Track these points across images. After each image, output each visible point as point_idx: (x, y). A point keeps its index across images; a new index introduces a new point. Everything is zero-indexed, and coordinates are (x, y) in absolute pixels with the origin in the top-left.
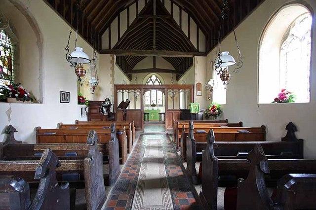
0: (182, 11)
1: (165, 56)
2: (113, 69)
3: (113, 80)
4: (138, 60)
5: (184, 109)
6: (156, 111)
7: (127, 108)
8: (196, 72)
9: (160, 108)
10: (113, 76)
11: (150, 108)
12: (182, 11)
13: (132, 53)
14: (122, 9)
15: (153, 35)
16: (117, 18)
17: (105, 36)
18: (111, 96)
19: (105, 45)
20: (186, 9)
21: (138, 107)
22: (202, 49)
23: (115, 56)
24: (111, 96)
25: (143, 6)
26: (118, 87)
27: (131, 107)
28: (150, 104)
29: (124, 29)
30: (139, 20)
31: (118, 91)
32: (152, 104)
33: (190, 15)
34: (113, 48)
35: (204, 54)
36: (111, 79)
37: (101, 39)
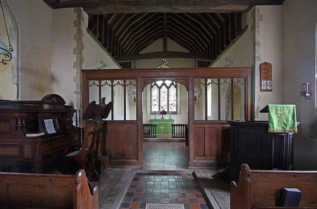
2: (79, 38)
3: (81, 60)
6: (166, 120)
7: (109, 118)
8: (259, 38)
9: (173, 117)
10: (79, 51)
11: (159, 117)
18: (76, 93)
21: (131, 116)
23: (85, 16)
24: (76, 93)
26: (89, 76)
27: (117, 115)
28: (158, 110)
31: (91, 82)
32: (161, 110)
36: (74, 58)
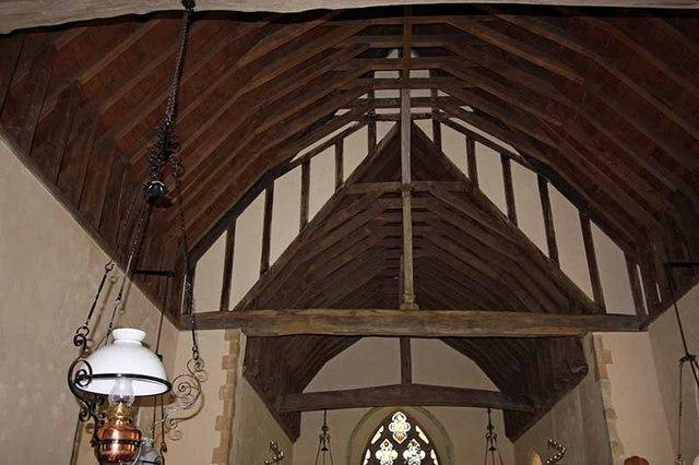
0: (513, 162)
1: (460, 332)
4: (326, 347)
5: (198, 332)
12: (513, 162)
13: (314, 321)
14: (285, 168)
15: (400, 248)
16: (262, 196)
17: (209, 265)
19: (206, 297)
20: (528, 157)
22: (618, 299)
23: (243, 338)
25: (255, 277)
29: (286, 234)
30: (341, 198)
33: (545, 176)
34: (238, 308)
35: (638, 323)
37: (191, 274)
